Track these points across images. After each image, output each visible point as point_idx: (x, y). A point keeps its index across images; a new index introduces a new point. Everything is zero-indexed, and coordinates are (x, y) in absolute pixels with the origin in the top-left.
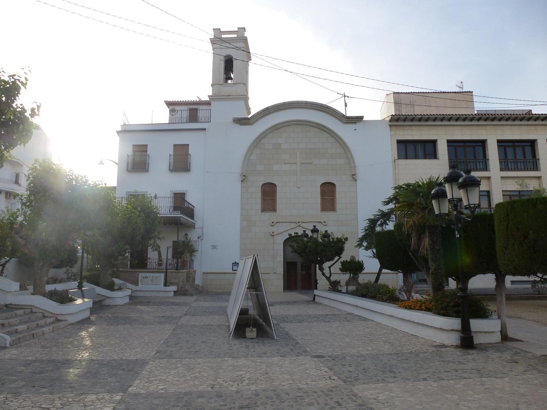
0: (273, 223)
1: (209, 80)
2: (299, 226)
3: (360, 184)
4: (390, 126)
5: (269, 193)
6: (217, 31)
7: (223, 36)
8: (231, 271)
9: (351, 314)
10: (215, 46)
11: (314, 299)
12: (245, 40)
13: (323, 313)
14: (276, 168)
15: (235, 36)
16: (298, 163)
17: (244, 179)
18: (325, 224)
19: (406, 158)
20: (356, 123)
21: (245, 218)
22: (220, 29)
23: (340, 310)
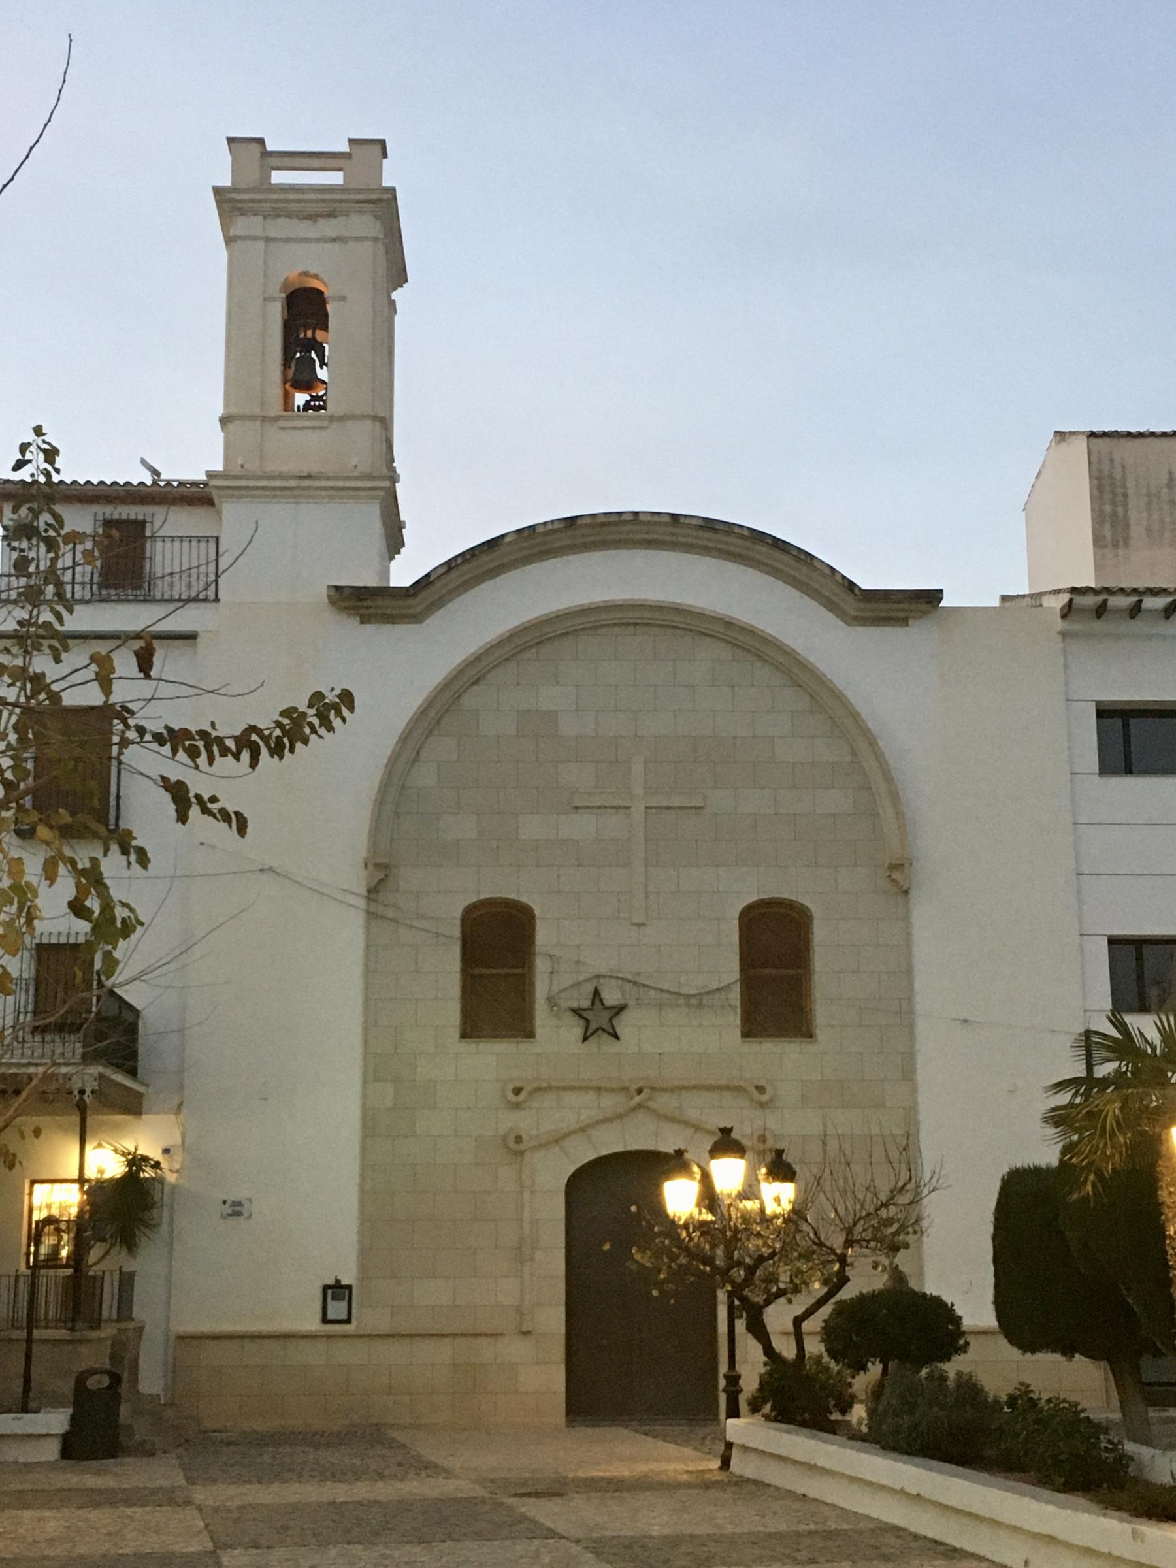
0: (517, 1091)
1: (211, 399)
2: (639, 1106)
3: (925, 916)
4: (1064, 635)
5: (497, 954)
6: (246, 148)
7: (279, 177)
8: (313, 1324)
9: (897, 1530)
10: (242, 226)
11: (726, 1463)
12: (385, 205)
13: (782, 1527)
14: (532, 827)
15: (335, 178)
16: (638, 809)
17: (381, 880)
18: (765, 1098)
19: (1129, 771)
20: (904, 622)
21: (384, 1061)
22: (260, 141)
23: (844, 1513)
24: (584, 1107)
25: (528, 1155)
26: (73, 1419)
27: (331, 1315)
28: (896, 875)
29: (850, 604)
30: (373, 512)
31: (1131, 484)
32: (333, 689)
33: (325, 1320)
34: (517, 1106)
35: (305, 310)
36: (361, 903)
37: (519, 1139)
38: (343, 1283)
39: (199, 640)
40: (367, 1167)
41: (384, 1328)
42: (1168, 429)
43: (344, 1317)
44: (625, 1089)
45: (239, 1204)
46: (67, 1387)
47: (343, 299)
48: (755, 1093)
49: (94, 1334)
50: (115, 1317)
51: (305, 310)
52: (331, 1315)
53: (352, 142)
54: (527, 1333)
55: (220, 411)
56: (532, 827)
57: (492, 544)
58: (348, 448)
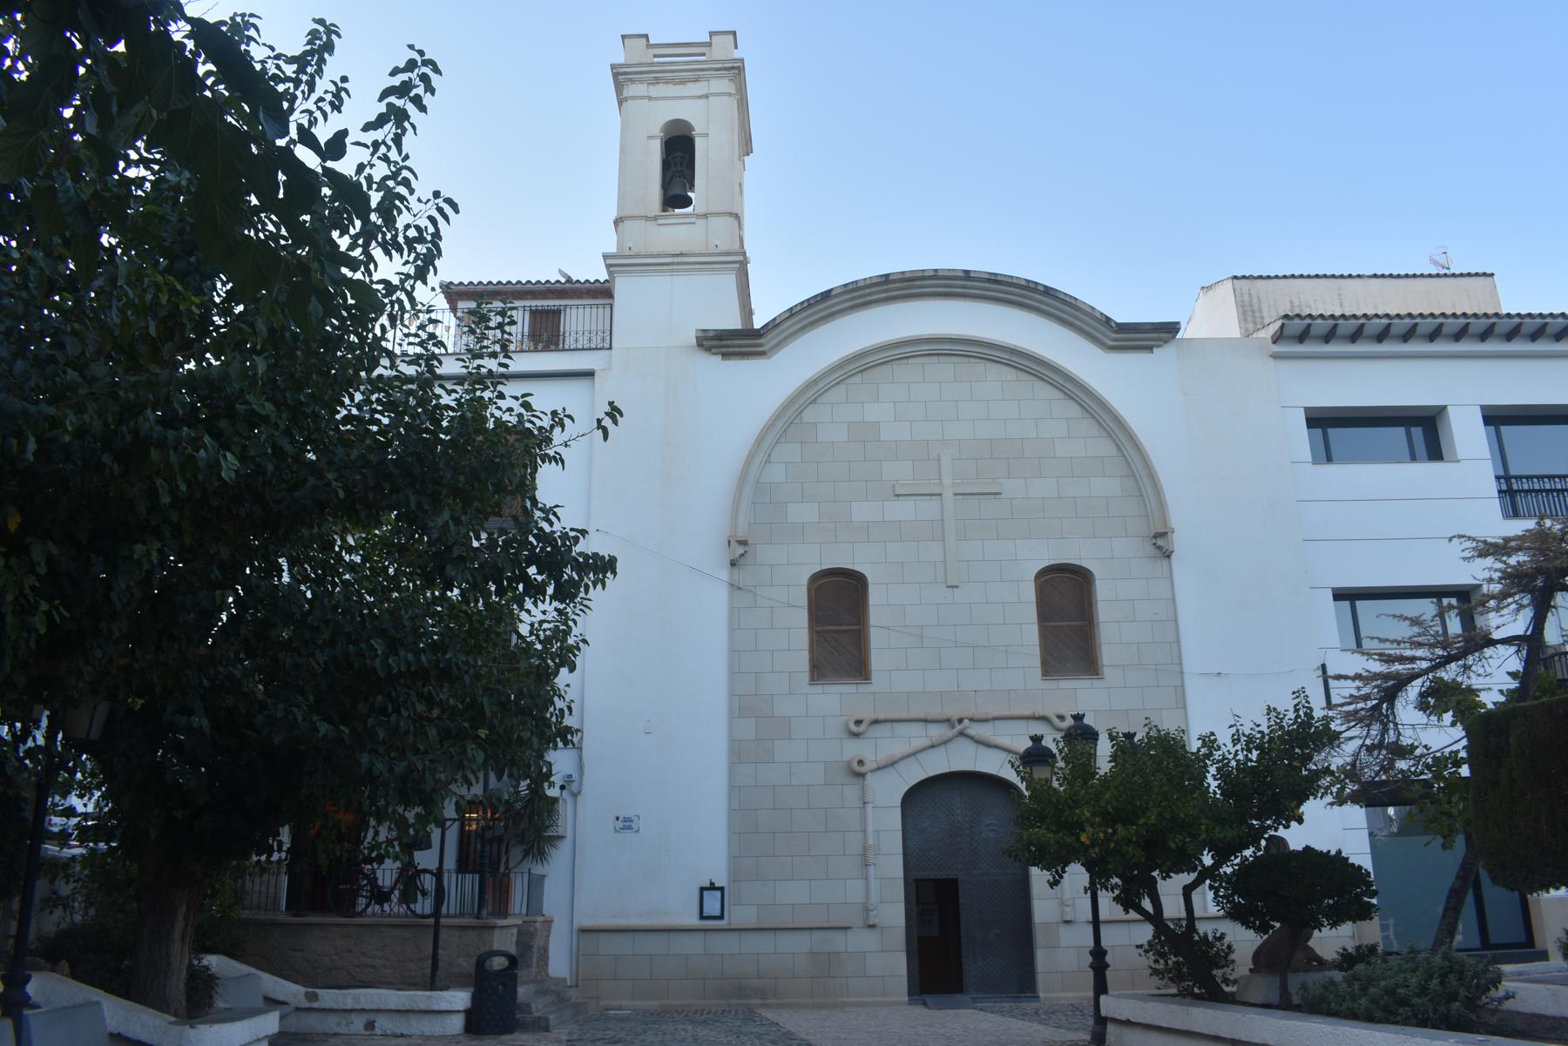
0: (858, 722)
5: (839, 603)
8: (693, 920)
16: (948, 494)
20: (1150, 349)
24: (917, 736)
26: (474, 999)
27: (707, 912)
28: (1160, 542)
29: (1109, 337)
30: (729, 281)
31: (1265, 310)
33: (702, 917)
34: (856, 735)
35: (679, 150)
36: (724, 574)
37: (861, 762)
40: (734, 788)
41: (753, 924)
43: (718, 913)
46: (467, 965)
48: (1057, 722)
49: (501, 922)
50: (524, 911)
51: (679, 150)
52: (707, 912)
53: (712, 34)
54: (872, 926)
55: (614, 215)
56: (862, 511)
57: (826, 295)
58: (718, 235)
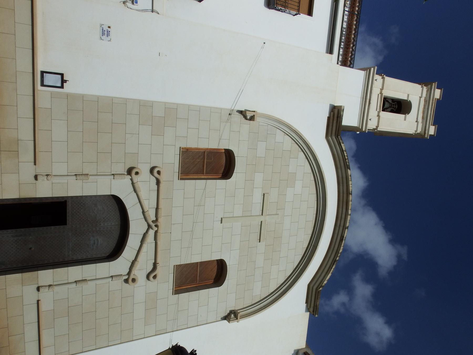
14: (259, 178)
18: (151, 277)
25: (129, 177)
32: (109, 27)
33: (43, 73)
37: (137, 173)
38: (64, 84)
39: (329, 55)
42: (30, 2)
43: (45, 83)
44: (157, 220)
45: (108, 35)
47: (405, 120)
54: (36, 177)
56: (259, 178)
